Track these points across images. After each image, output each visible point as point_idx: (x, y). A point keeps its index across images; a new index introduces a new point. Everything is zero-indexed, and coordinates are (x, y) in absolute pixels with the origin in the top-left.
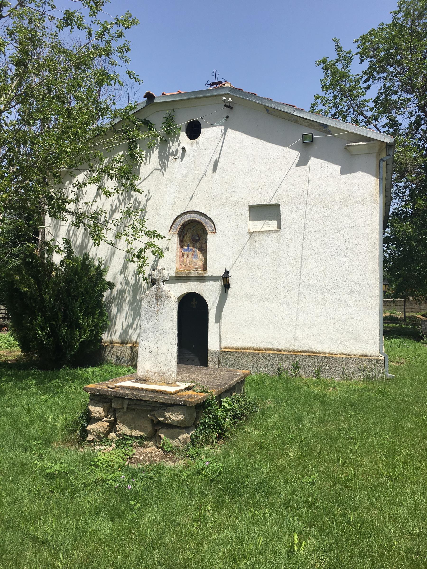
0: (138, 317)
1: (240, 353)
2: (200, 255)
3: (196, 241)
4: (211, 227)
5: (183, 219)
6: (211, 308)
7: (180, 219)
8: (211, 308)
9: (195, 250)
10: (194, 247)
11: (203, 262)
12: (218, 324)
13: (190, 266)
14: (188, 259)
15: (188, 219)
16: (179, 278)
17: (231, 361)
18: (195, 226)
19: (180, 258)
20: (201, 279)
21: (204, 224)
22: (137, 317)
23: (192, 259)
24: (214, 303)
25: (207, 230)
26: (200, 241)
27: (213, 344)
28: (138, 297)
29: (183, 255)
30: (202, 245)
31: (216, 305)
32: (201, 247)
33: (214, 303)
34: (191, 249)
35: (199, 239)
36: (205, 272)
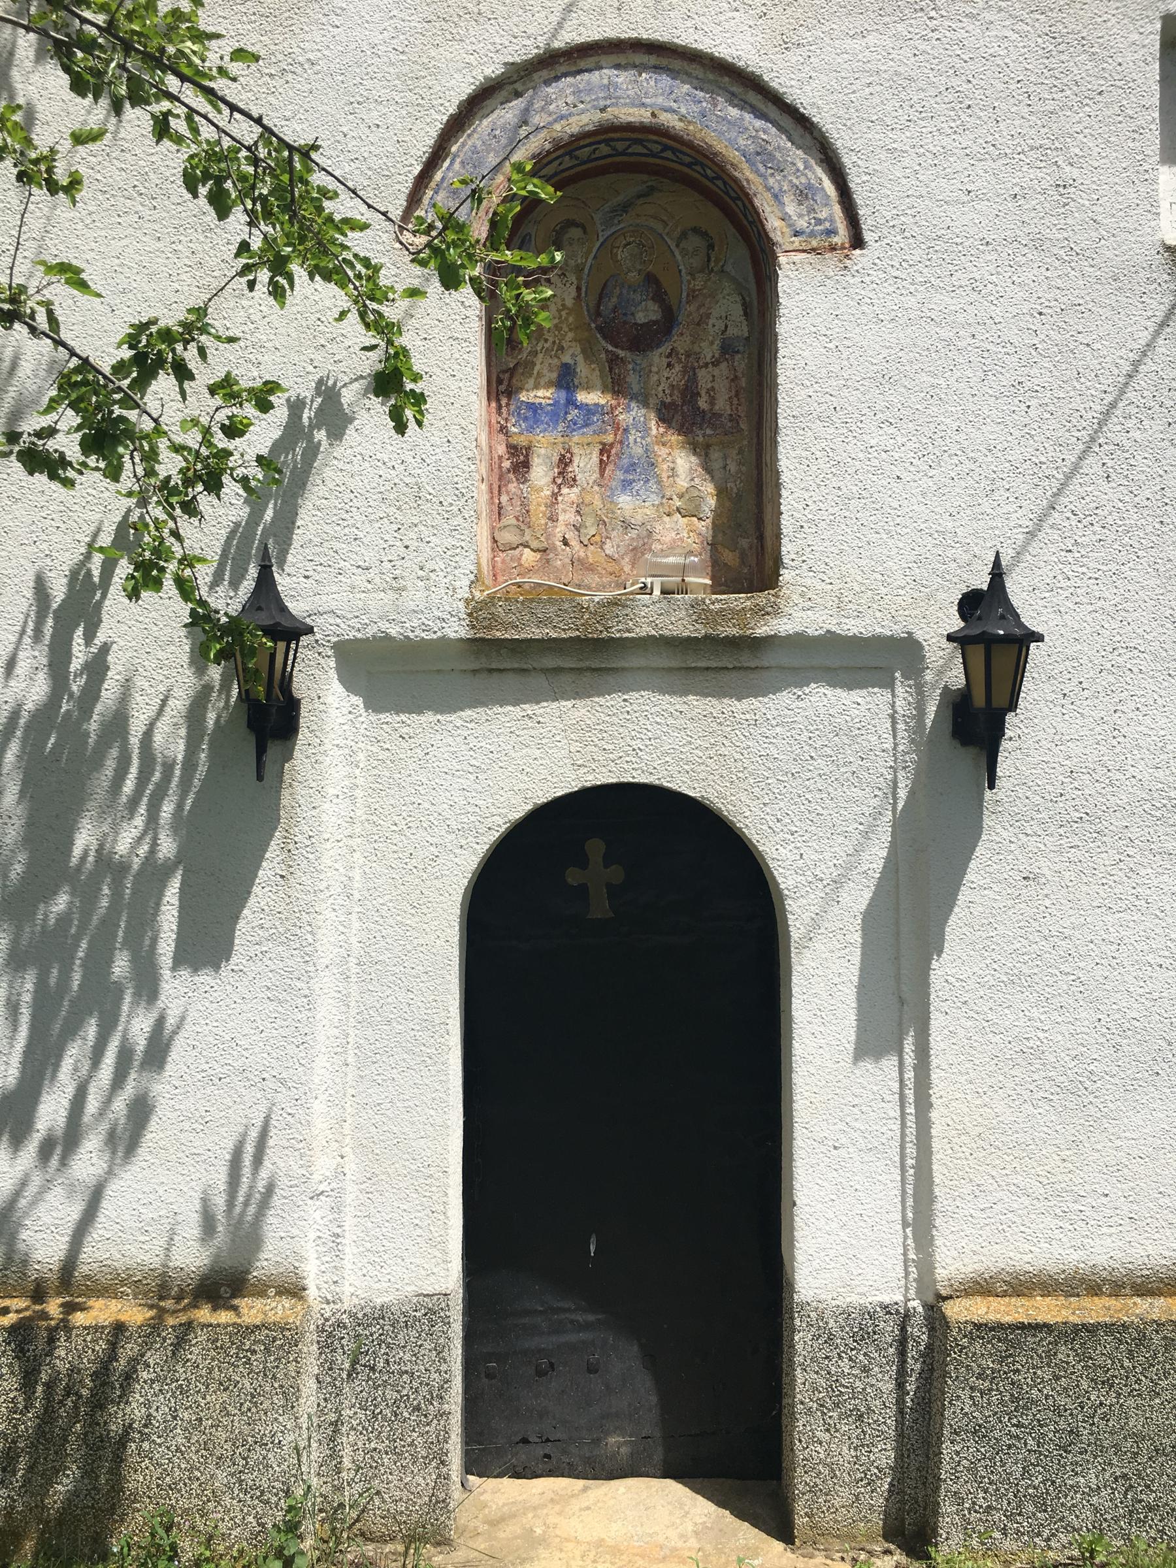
0: (91, 1030)
1: (1142, 1339)
2: (681, 466)
3: (643, 340)
4: (804, 194)
5: (537, 119)
6: (815, 924)
7: (505, 114)
8: (815, 924)
9: (632, 414)
10: (617, 387)
11: (704, 527)
12: (889, 1064)
13: (592, 555)
14: (570, 494)
15: (584, 120)
16: (514, 655)
17: (1058, 1411)
18: (625, 207)
19: (497, 488)
20: (726, 661)
21: (746, 174)
22: (72, 1030)
23: (608, 500)
24: (838, 883)
25: (774, 224)
26: (680, 341)
27: (842, 1248)
28: (84, 839)
29: (520, 461)
30: (690, 373)
31: (858, 897)
32: (690, 392)
33: (838, 883)
34: (589, 411)
35: (668, 323)
36: (761, 598)
